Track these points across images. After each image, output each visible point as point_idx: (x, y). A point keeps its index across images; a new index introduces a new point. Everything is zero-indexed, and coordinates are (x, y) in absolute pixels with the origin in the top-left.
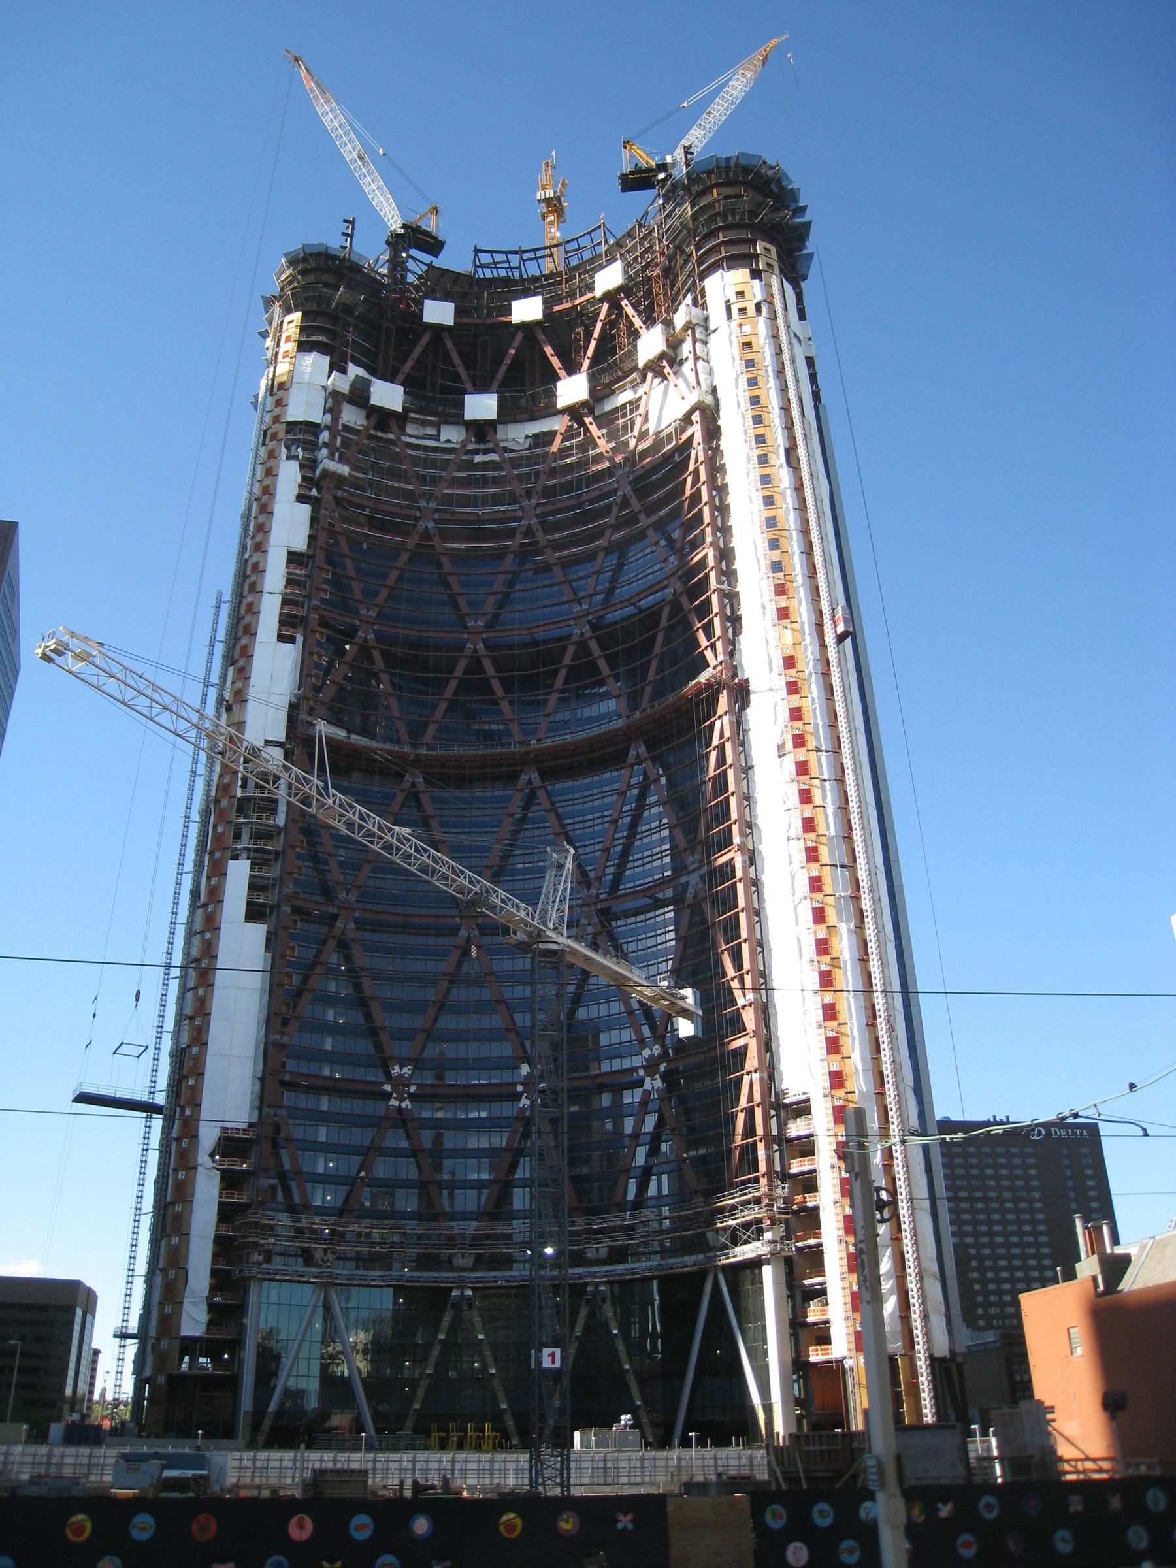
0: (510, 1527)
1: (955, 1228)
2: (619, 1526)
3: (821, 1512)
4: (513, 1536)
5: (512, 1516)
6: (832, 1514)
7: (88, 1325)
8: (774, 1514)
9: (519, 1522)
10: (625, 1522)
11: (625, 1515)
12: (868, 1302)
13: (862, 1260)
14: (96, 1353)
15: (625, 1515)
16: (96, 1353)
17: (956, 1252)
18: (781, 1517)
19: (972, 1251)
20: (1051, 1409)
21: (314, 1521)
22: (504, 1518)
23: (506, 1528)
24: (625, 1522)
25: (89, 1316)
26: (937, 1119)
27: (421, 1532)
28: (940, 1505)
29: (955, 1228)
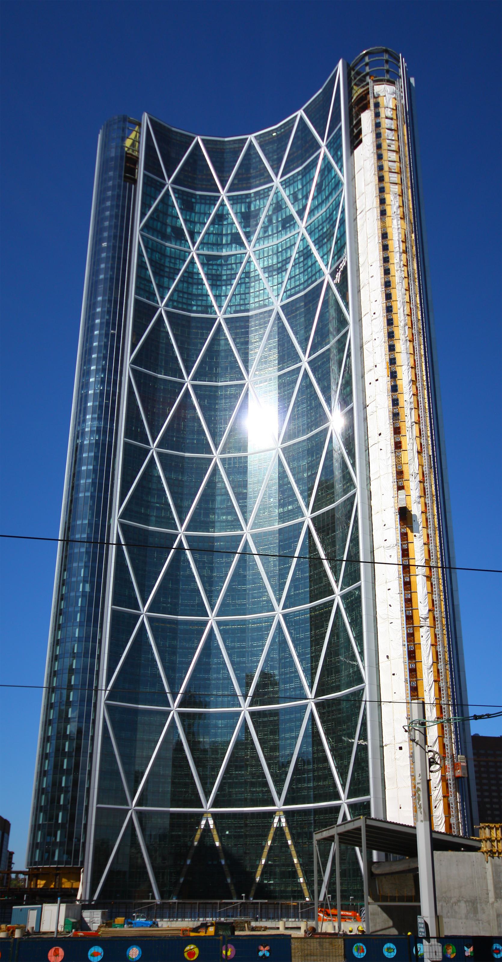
0: (191, 954)
1: (479, 793)
2: (261, 954)
3: (388, 949)
4: (192, 959)
5: (192, 946)
6: (395, 951)
7: (5, 839)
8: (358, 949)
9: (197, 951)
10: (264, 951)
11: (264, 947)
12: (422, 821)
13: (419, 795)
14: (11, 854)
15: (264, 947)
16: (11, 854)
17: (479, 805)
18: (363, 951)
19: (488, 806)
20: (13, 864)
21: (64, 950)
22: (188, 948)
23: (188, 954)
24: (264, 951)
25: (6, 835)
26: (472, 734)
27: (134, 957)
28: (466, 948)
29: (479, 793)
